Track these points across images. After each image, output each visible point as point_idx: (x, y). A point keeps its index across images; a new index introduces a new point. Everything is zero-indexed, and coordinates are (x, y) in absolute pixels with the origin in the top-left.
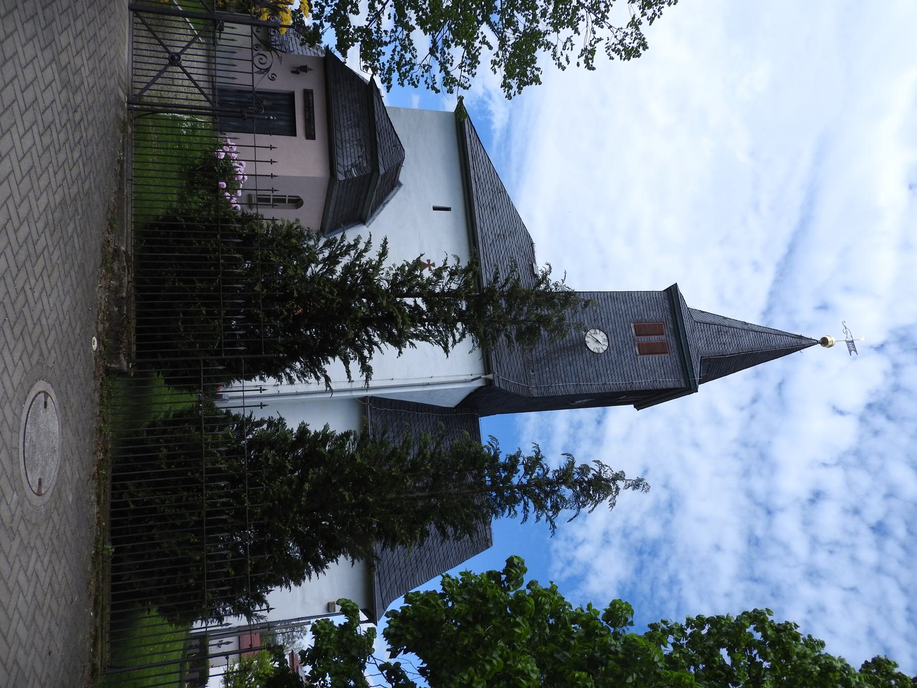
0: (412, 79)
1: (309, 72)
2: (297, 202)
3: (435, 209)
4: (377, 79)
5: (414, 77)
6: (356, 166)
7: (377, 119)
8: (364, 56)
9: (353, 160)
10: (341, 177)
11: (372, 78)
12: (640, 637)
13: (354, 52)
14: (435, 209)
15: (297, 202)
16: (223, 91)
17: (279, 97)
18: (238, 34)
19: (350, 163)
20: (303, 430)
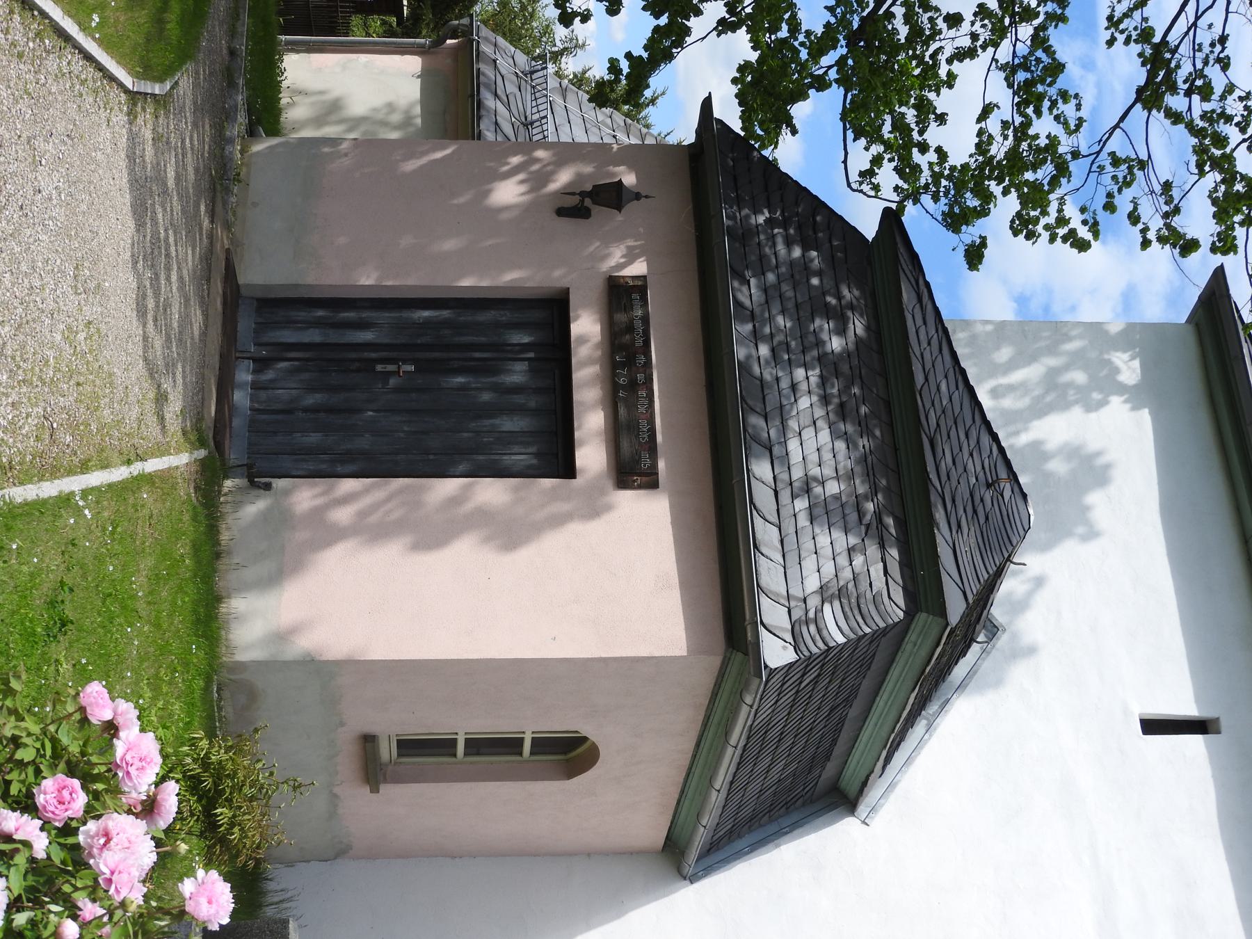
0: (1062, 221)
1: (632, 207)
2: (568, 754)
3: (1152, 726)
4: (921, 223)
5: (1071, 211)
6: (841, 593)
7: (919, 379)
8: (858, 121)
9: (828, 569)
10: (776, 653)
11: (891, 219)
12: (766, 666)
13: (818, 112)
14: (1152, 726)
15: (568, 754)
16: (278, 306)
17: (505, 316)
18: (356, 84)
19: (812, 584)
20: (221, 926)
